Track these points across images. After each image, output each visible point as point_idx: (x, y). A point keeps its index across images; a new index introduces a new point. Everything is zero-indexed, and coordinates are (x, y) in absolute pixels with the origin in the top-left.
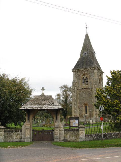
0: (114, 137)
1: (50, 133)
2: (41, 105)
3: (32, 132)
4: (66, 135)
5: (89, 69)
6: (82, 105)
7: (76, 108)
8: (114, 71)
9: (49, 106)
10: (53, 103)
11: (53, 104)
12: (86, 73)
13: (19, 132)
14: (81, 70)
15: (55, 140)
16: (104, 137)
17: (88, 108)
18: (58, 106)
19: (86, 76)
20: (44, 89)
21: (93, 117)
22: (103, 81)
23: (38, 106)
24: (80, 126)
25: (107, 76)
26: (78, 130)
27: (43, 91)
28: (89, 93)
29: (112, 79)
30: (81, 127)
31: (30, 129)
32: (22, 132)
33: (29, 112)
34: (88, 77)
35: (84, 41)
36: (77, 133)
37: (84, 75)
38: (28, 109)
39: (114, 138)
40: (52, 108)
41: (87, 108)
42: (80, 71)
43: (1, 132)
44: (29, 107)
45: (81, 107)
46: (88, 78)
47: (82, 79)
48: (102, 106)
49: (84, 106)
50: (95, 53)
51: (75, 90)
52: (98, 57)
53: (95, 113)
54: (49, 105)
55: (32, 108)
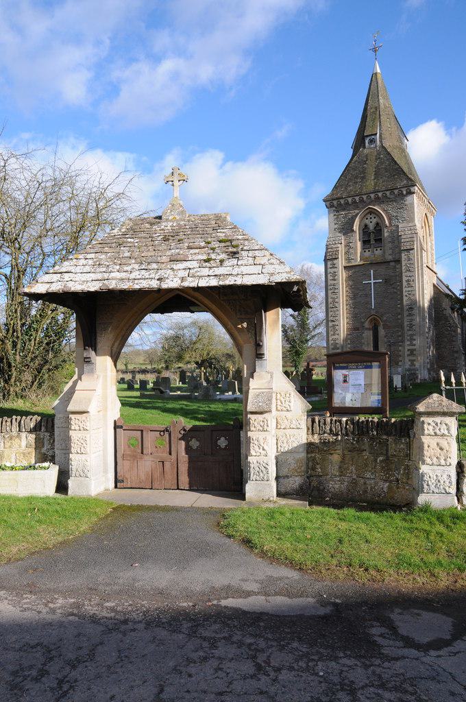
1: (223, 442)
2: (154, 266)
5: (388, 193)
10: (235, 253)
11: (234, 254)
14: (357, 199)
17: (382, 332)
19: (374, 221)
21: (400, 363)
23: (135, 275)
36: (395, 446)
37: (369, 216)
42: (354, 202)
44: (79, 277)
49: (367, 325)
53: (415, 345)
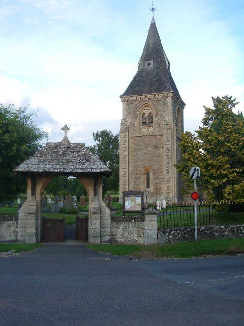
0: (217, 234)
3: (39, 222)
4: (114, 229)
6: (140, 170)
7: (127, 175)
8: (218, 97)
9: (78, 167)
11: (88, 161)
12: (150, 103)
13: (12, 222)
15: (91, 240)
16: (198, 235)
18: (100, 167)
19: (149, 111)
20: (69, 129)
22: (183, 123)
24: (146, 211)
25: (204, 107)
26: (143, 220)
27: (66, 133)
28: (155, 146)
29: (213, 112)
30: (150, 213)
31: (37, 216)
32: (19, 222)
33: (34, 176)
34: (154, 114)
35: (147, 34)
36: (139, 224)
37: (146, 108)
38: (34, 172)
39: (218, 237)
40: (87, 170)
41: (149, 176)
43: (5, 255)
45: (137, 174)
46: (154, 115)
47: (141, 117)
48: (197, 168)
50: (169, 64)
51: (125, 139)
52: (175, 72)
54: (79, 162)
55: (41, 170)
